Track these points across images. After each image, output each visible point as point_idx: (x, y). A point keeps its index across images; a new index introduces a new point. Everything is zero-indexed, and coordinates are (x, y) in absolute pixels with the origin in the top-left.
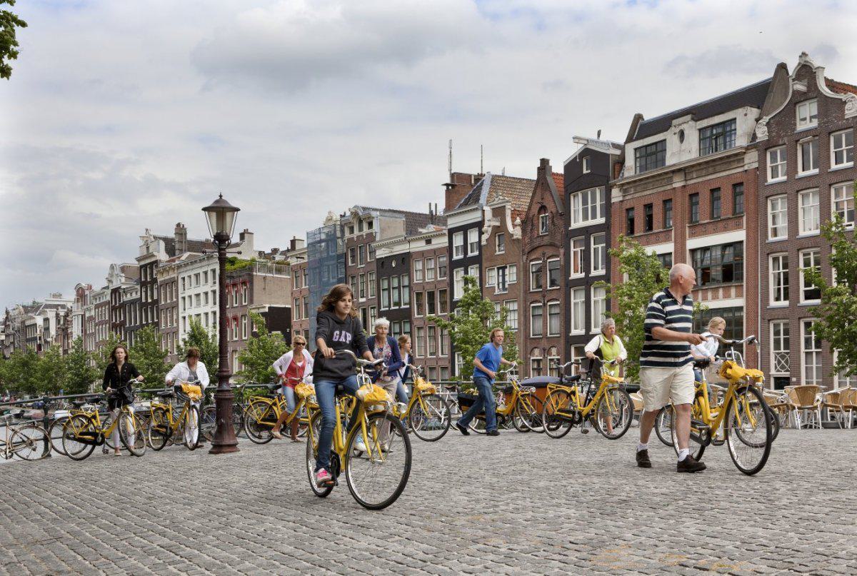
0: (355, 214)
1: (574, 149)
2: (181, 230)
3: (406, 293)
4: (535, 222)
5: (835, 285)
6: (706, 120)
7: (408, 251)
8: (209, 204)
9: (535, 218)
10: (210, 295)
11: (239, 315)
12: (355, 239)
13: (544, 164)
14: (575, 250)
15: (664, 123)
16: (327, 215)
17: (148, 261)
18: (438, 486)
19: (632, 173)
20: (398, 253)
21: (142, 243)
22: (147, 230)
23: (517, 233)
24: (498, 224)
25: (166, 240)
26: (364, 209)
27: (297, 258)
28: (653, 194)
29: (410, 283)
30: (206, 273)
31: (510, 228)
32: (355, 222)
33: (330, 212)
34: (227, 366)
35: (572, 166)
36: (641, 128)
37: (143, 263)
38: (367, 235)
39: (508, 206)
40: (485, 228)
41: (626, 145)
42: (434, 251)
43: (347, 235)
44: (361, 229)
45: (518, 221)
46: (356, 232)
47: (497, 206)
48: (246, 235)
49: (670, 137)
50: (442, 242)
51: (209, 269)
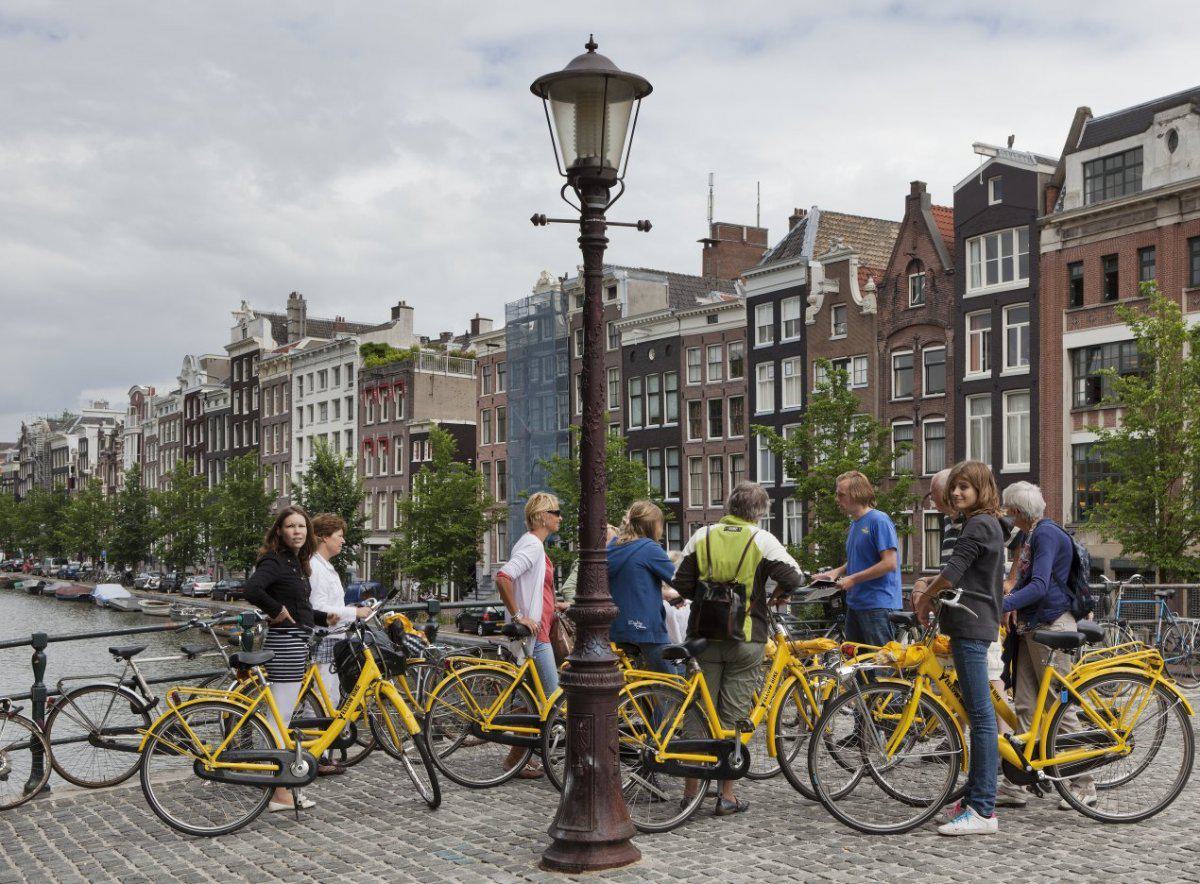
1: (975, 164)
2: (297, 303)
8: (558, 64)
13: (918, 192)
14: (974, 333)
15: (1138, 119)
19: (1079, 204)
23: (870, 304)
25: (272, 318)
28: (1119, 238)
35: (969, 194)
36: (1088, 131)
37: (236, 354)
45: (871, 284)
49: (1152, 143)
50: (740, 318)
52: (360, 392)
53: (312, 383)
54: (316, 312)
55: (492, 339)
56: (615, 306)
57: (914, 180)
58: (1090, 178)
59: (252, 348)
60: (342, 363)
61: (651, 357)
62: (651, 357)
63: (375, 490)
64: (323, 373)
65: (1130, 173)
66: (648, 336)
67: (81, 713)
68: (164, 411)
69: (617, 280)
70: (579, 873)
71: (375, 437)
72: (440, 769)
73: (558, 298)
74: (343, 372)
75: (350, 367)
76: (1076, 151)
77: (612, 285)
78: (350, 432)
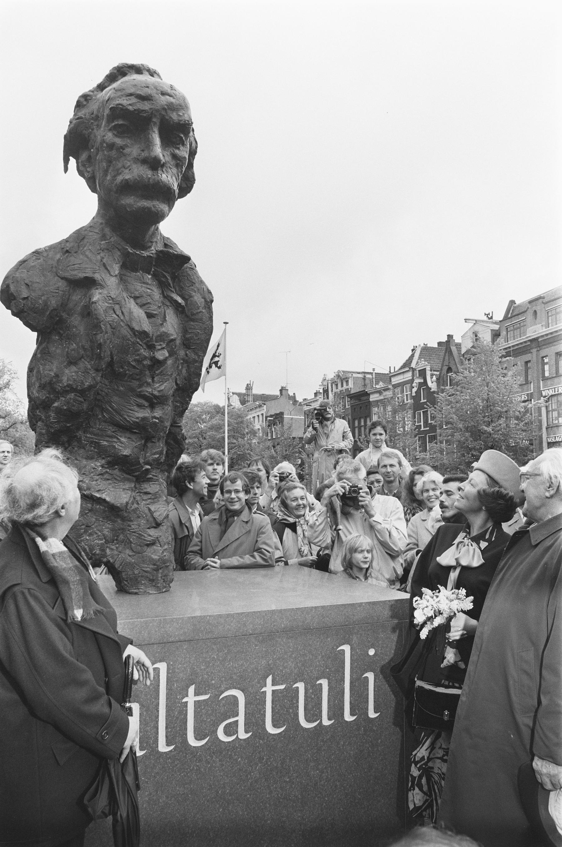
0: (338, 376)
4: (445, 379)
6: (349, 687)
9: (445, 377)
16: (323, 376)
18: (346, 638)
19: (228, 486)
24: (422, 381)
25: (239, 395)
26: (343, 372)
30: (258, 416)
31: (430, 384)
38: (345, 390)
39: (428, 368)
40: (414, 385)
44: (342, 386)
45: (434, 378)
46: (340, 388)
51: (256, 415)
54: (256, 391)
57: (439, 341)
58: (364, 379)
60: (260, 413)
65: (522, 328)
67: (552, 627)
68: (339, 385)
70: (225, 727)
72: (540, 725)
73: (330, 385)
74: (260, 416)
75: (262, 414)
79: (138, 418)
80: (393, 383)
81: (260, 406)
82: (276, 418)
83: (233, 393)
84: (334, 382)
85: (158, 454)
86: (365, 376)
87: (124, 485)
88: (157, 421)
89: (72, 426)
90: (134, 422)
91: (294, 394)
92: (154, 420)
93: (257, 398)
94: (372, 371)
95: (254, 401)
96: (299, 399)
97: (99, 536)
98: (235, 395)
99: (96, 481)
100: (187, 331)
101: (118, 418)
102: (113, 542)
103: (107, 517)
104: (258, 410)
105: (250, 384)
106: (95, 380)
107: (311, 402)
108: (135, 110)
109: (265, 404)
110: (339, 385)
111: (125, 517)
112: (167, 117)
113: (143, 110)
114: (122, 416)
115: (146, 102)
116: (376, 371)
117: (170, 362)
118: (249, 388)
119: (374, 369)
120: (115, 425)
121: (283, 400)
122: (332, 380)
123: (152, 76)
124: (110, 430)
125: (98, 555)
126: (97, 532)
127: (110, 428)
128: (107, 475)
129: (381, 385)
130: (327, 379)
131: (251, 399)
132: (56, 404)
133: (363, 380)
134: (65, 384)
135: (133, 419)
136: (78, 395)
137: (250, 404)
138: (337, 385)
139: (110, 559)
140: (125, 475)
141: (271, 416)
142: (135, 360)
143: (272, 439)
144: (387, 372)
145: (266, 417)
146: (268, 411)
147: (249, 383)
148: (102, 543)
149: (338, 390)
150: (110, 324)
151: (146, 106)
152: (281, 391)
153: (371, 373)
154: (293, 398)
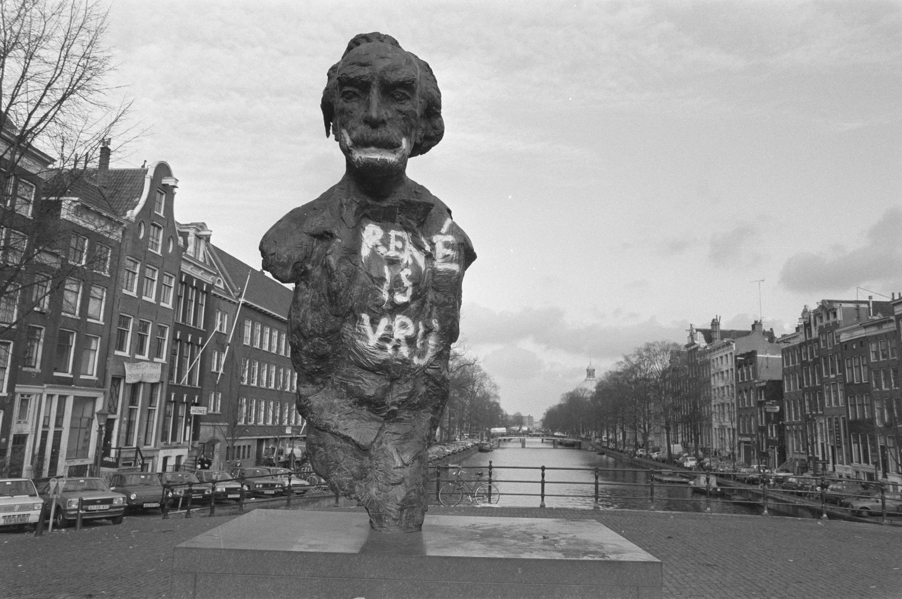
3: (864, 370)
5: (793, 420)
7: (864, 335)
10: (730, 372)
11: (748, 387)
12: (824, 327)
16: (803, 308)
17: (692, 347)
20: (857, 337)
21: (688, 334)
22: (691, 325)
27: (784, 343)
29: (867, 363)
30: (726, 355)
32: (823, 313)
33: (805, 306)
34: (220, 483)
37: (689, 349)
38: (833, 323)
41: (411, 161)
42: (886, 334)
43: (818, 323)
44: (828, 318)
46: (825, 321)
47: (162, 295)
48: (756, 326)
51: (723, 354)
52: (736, 366)
53: (727, 360)
54: (723, 327)
55: (787, 339)
56: (836, 322)
58: (858, 309)
59: (695, 346)
60: (728, 353)
61: (854, 347)
62: (854, 347)
63: (749, 414)
64: (721, 357)
66: (803, 502)
68: (825, 318)
69: (836, 309)
71: (743, 388)
73: (812, 317)
76: (267, 551)
77: (834, 311)
78: (732, 386)
79: (380, 360)
80: (896, 314)
81: (728, 344)
82: (748, 358)
83: (697, 330)
84: (817, 313)
85: (406, 395)
86: (858, 306)
87: (371, 425)
88: (400, 363)
89: (323, 367)
90: (376, 364)
91: (771, 329)
92: (397, 362)
93: (725, 334)
94: (868, 299)
95: (722, 339)
96: (778, 335)
97: (347, 473)
98: (698, 333)
99: (344, 420)
100: (434, 274)
101: (362, 361)
102: (362, 479)
103: (355, 455)
104: (726, 348)
105: (717, 319)
106: (334, 325)
107: (790, 339)
108: (356, 77)
109: (733, 342)
110: (825, 318)
111: (372, 456)
112: (385, 78)
113: (363, 76)
114: (365, 359)
115: (366, 68)
116: (874, 299)
117: (412, 306)
118: (715, 323)
119: (870, 297)
120: (360, 367)
121: (756, 337)
122: (815, 311)
123: (382, 41)
124: (357, 372)
125: (347, 491)
126: (346, 469)
127: (356, 369)
128: (355, 415)
129: (878, 317)
130: (808, 310)
131: (718, 335)
132: (305, 348)
133: (856, 311)
134: (310, 329)
135: (375, 362)
136: (322, 339)
137: (717, 342)
138: (821, 318)
139: (359, 496)
140: (373, 415)
141: (741, 355)
142: (374, 305)
143: (744, 382)
144: (889, 300)
145: (736, 357)
146: (737, 350)
147: (715, 318)
148: (350, 480)
149: (824, 324)
150: (345, 273)
151: (366, 71)
152: (753, 326)
153: (867, 303)
154: (770, 335)
